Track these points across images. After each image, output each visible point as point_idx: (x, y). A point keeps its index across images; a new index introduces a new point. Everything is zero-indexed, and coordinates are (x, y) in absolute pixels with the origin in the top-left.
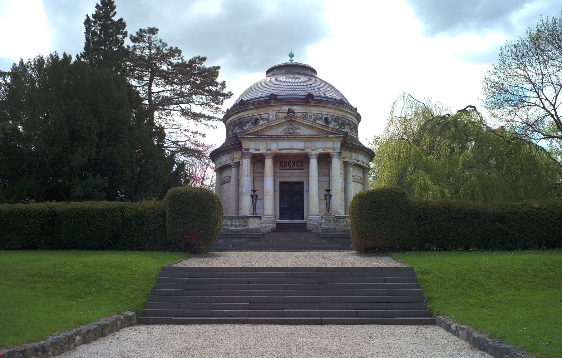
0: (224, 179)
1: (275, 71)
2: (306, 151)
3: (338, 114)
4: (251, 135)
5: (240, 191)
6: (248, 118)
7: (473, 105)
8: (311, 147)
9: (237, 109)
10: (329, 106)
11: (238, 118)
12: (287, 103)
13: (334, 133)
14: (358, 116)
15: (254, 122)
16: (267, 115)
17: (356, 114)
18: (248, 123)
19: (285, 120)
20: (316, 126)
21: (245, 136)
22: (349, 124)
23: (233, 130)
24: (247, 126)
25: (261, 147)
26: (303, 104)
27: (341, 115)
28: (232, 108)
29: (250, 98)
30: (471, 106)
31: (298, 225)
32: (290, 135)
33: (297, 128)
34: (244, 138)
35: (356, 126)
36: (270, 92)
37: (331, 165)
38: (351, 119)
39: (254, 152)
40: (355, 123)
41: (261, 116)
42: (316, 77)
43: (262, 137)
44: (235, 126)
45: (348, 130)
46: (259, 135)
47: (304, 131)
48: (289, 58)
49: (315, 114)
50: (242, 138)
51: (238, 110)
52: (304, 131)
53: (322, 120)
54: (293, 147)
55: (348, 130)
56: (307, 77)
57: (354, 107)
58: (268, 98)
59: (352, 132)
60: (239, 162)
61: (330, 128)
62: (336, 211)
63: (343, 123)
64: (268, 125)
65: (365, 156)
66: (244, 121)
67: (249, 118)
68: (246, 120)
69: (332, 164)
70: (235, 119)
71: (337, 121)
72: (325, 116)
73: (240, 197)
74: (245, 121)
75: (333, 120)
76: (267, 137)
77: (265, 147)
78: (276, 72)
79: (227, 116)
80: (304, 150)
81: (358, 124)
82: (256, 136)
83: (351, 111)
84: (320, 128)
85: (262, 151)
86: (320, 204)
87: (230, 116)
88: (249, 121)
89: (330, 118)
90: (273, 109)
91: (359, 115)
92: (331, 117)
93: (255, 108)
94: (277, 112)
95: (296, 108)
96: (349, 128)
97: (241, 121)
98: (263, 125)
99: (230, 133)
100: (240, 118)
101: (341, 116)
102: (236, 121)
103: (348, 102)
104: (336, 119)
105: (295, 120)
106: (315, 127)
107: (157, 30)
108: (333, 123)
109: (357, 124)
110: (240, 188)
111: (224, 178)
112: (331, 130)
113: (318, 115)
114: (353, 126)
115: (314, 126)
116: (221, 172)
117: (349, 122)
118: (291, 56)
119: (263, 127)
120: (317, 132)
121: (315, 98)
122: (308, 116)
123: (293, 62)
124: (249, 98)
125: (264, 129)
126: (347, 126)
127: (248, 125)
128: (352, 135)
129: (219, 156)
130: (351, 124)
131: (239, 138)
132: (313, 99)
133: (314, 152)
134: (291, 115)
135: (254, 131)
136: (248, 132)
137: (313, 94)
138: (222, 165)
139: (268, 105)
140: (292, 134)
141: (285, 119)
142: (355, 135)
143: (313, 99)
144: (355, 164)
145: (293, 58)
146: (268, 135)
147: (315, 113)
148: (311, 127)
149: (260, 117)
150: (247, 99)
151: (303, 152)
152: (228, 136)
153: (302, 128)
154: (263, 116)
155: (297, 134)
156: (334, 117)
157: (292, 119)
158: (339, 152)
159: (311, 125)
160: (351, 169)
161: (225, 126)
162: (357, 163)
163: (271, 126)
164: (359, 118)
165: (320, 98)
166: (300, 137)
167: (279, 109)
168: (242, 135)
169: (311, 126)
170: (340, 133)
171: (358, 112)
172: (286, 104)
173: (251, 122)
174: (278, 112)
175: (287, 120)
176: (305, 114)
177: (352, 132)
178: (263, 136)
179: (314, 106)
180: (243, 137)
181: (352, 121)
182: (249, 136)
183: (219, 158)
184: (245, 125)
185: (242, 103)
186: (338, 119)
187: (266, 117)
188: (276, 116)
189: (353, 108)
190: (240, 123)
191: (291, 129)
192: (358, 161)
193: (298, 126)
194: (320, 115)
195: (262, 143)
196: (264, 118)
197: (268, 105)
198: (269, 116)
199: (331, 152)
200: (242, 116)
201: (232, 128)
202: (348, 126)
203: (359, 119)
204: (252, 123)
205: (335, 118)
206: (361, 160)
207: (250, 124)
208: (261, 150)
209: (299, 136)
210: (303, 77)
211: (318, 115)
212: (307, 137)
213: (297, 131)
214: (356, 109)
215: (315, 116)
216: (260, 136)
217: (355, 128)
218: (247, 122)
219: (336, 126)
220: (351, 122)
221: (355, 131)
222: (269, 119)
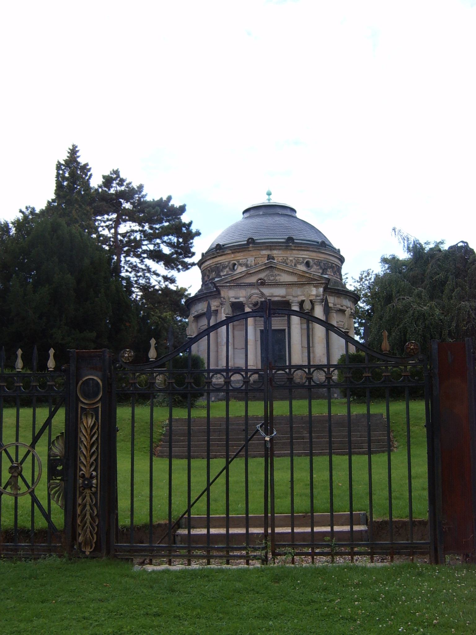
0: (201, 328)
1: (252, 212)
2: (288, 298)
3: (320, 257)
4: (230, 283)
5: (219, 340)
6: (224, 263)
7: (465, 241)
8: (292, 294)
9: (213, 254)
10: (311, 250)
11: (215, 263)
12: (267, 248)
13: (316, 279)
14: (341, 258)
15: (231, 267)
16: (245, 260)
17: (340, 256)
18: (225, 269)
19: (265, 267)
20: (297, 272)
21: (223, 285)
22: (332, 267)
23: (208, 276)
24: (224, 272)
25: (241, 295)
26: (283, 248)
27: (323, 258)
28: (206, 253)
29: (227, 242)
30: (462, 242)
31: (281, 375)
32: (270, 282)
33: (278, 275)
34: (223, 286)
35: (339, 269)
36: (248, 236)
37: (314, 312)
38: (334, 261)
39: (234, 300)
40: (338, 266)
41: (239, 261)
42: (296, 217)
43: (242, 284)
44: (211, 271)
45: (331, 273)
46: (239, 283)
47: (285, 278)
48: (267, 197)
49: (296, 258)
50: (221, 286)
51: (214, 255)
52: (285, 278)
53: (303, 264)
54: (274, 295)
55: (331, 273)
56: (286, 219)
57: (337, 248)
58: (246, 242)
59: (336, 276)
60: (217, 310)
61: (312, 275)
62: (320, 360)
63: (325, 267)
64: (247, 272)
65: (349, 300)
66: (221, 267)
67: (227, 263)
68: (223, 266)
69: (315, 311)
70: (212, 264)
71: (319, 265)
72: (307, 260)
73: (219, 347)
74: (223, 267)
75: (315, 263)
76: (246, 285)
77: (245, 295)
78: (253, 213)
79: (203, 261)
80: (285, 297)
81: (342, 266)
82: (235, 284)
83: (333, 253)
84: (301, 274)
85: (241, 299)
86: (302, 352)
87: (206, 261)
88: (226, 267)
89: (311, 261)
90: (252, 253)
91: (342, 256)
92: (313, 261)
93: (232, 253)
94: (255, 256)
95: (275, 253)
96: (332, 271)
97: (218, 267)
98: (242, 273)
99: (206, 278)
100: (217, 263)
101: (323, 259)
102: (212, 266)
103: (331, 243)
104: (318, 263)
105: (275, 266)
106: (296, 273)
107: (132, 182)
108: (315, 267)
109: (340, 266)
110: (219, 337)
111: (201, 326)
112: (313, 276)
113: (299, 259)
114: (336, 269)
115: (295, 272)
116: (197, 320)
117: (332, 265)
118: (269, 194)
119: (242, 274)
120: (298, 279)
121: (296, 241)
122: (289, 260)
123: (271, 201)
124: (225, 242)
125: (244, 276)
126: (330, 269)
127: (225, 270)
128: (335, 278)
129: (195, 304)
130: (334, 266)
131: (218, 286)
132: (293, 243)
133: (296, 299)
134: (271, 261)
135: (233, 279)
136: (227, 281)
137: (293, 237)
138: (198, 313)
139: (247, 250)
140: (273, 281)
141: (265, 265)
142: (339, 277)
143: (293, 243)
144: (338, 309)
145: (271, 197)
146: (247, 283)
147: (295, 257)
148: (293, 273)
149: (238, 263)
150: (224, 243)
151: (284, 299)
152: (204, 281)
153: (283, 274)
154: (241, 261)
155: (278, 281)
156: (316, 260)
157: (272, 265)
158: (321, 299)
159: (292, 271)
160: (335, 314)
161: (200, 271)
162: (341, 308)
163: (250, 274)
164: (342, 260)
165: (301, 241)
166: (281, 284)
167: (258, 254)
168: (221, 284)
169: (292, 272)
170: (322, 279)
171: (342, 253)
172: (265, 248)
173: (228, 267)
174: (257, 256)
175: (267, 267)
176: (285, 258)
177: (336, 276)
178: (242, 283)
179: (294, 250)
180: (221, 285)
181: (335, 263)
182: (228, 285)
183: (196, 305)
184: (222, 271)
185: (218, 247)
186: (320, 263)
187: (245, 262)
188: (255, 261)
189: (336, 249)
190: (217, 269)
191: (272, 276)
192: (342, 306)
193: (278, 273)
194: (301, 259)
195: (242, 291)
196: (242, 263)
197: (247, 250)
198: (248, 261)
199: (314, 299)
200: (219, 261)
201: (208, 273)
202: (331, 269)
203: (342, 261)
204: (230, 268)
205: (317, 262)
206: (345, 305)
207: (227, 269)
208: (240, 298)
209: (280, 283)
210: (282, 218)
211: (299, 259)
212: (289, 284)
213: (278, 278)
214: (339, 251)
215: (296, 261)
216: (240, 284)
217: (338, 270)
218: (224, 268)
219: (318, 269)
220: (334, 265)
221: (338, 274)
222: (247, 264)
